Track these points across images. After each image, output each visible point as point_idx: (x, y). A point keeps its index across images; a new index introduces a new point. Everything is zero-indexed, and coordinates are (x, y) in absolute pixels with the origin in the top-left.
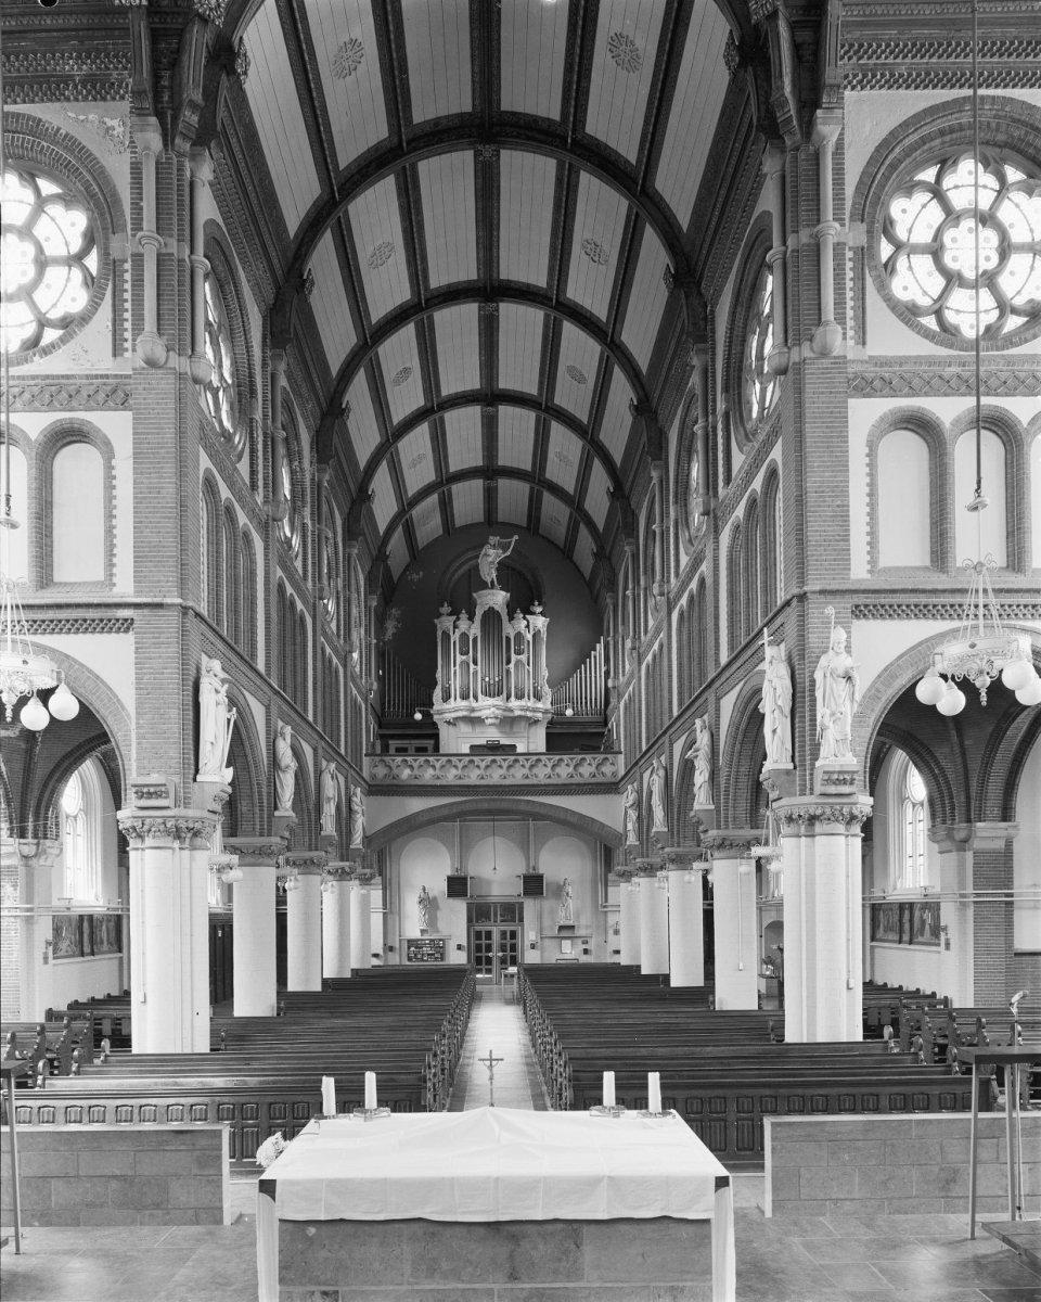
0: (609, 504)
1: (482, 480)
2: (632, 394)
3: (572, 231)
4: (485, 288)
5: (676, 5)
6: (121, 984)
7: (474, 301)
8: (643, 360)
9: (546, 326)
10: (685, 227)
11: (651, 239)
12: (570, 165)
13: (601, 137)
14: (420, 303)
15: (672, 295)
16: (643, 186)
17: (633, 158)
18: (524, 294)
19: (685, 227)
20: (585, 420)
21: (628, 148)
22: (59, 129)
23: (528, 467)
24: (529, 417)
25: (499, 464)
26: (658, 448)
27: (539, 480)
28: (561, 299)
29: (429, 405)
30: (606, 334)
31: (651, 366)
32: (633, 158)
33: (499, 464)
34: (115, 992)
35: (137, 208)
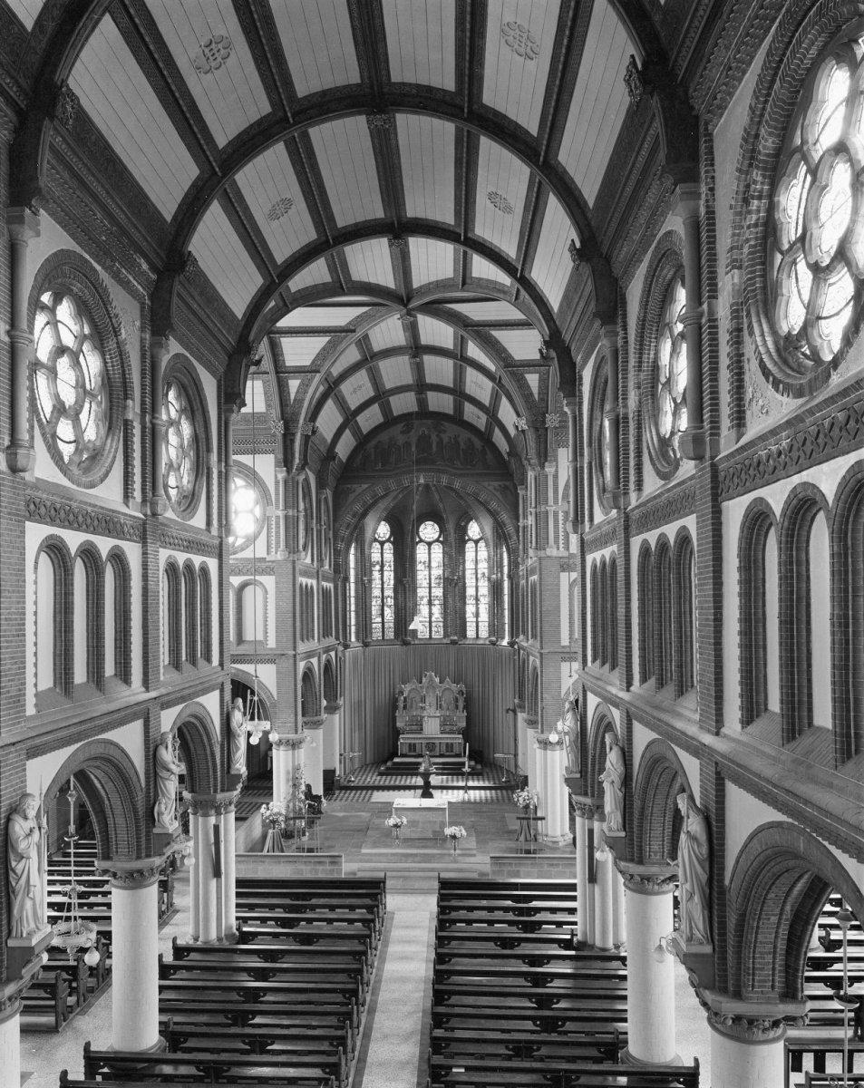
0: (626, 100)
1: (362, 119)
2: (574, 235)
3: (483, 49)
4: (393, 223)
5: (573, 4)
6: (293, 762)
7: (360, 113)
8: (590, 191)
9: (455, 370)
10: (591, 203)
11: (556, 215)
12: (468, 131)
13: (500, 108)
14: (328, 241)
15: (576, 269)
16: (545, 157)
17: (534, 131)
18: (425, 100)
19: (591, 203)
20: (533, 129)
21: (529, 119)
22: (625, 1020)
23: (449, 84)
24: (443, 131)
25: (409, 215)
26: (610, 308)
27: (471, 111)
28: (470, 235)
29: (324, 238)
30: (538, 152)
31: (599, 198)
32: (534, 131)
33: (409, 215)
34: (723, 730)
35: (277, 500)
